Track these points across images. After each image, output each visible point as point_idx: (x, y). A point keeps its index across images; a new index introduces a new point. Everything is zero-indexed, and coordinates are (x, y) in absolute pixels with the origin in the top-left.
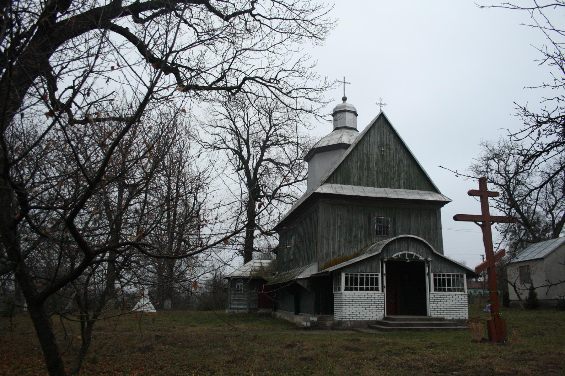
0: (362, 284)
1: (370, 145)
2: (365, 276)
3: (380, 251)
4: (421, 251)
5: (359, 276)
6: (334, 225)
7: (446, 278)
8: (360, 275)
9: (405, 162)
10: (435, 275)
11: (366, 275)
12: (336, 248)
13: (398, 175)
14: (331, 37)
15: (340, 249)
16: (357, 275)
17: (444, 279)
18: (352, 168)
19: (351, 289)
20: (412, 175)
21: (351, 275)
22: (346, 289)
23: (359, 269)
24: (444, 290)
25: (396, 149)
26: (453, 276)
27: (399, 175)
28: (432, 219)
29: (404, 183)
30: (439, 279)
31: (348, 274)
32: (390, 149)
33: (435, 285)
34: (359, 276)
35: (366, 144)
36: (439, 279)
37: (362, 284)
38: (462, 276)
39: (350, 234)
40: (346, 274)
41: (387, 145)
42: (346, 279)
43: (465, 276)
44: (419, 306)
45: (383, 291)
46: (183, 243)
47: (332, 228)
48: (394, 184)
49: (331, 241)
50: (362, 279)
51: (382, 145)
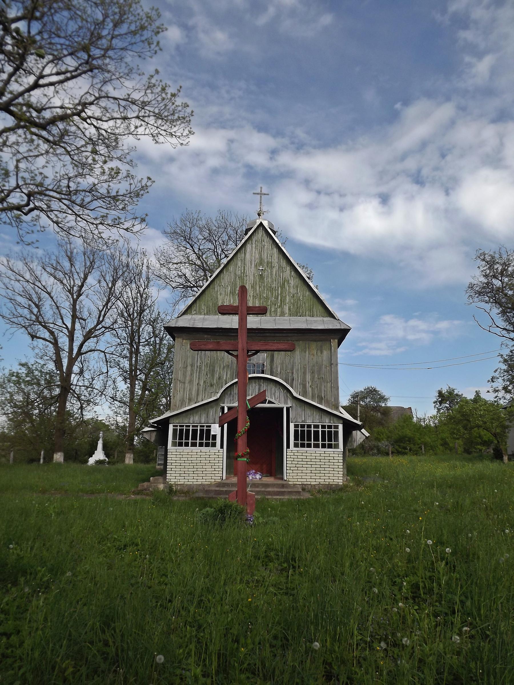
0: (194, 437)
1: (244, 264)
2: (199, 428)
3: (218, 395)
4: (277, 394)
5: (191, 428)
6: (192, 365)
7: (320, 429)
8: (193, 426)
9: (292, 282)
10: (296, 426)
11: (201, 426)
12: (193, 393)
13: (281, 300)
14: (434, 396)
15: (198, 395)
16: (189, 426)
17: (309, 432)
18: (221, 294)
19: (303, 446)
20: (301, 298)
21: (180, 426)
22: (296, 445)
23: (191, 419)
24: (309, 446)
25: (280, 267)
26: (323, 427)
27: (283, 301)
28: (326, 353)
29: (289, 309)
30: (303, 432)
31: (177, 426)
32: (272, 267)
33: (296, 438)
34: (191, 428)
35: (239, 264)
36: (303, 432)
37: (194, 437)
38: (337, 427)
39: (213, 376)
40: (174, 426)
41: (268, 263)
42: (175, 431)
43: (341, 427)
44: (273, 465)
45: (222, 447)
46: (147, 392)
47: (189, 368)
48: (276, 311)
49: (187, 385)
50: (195, 432)
51: (261, 263)
